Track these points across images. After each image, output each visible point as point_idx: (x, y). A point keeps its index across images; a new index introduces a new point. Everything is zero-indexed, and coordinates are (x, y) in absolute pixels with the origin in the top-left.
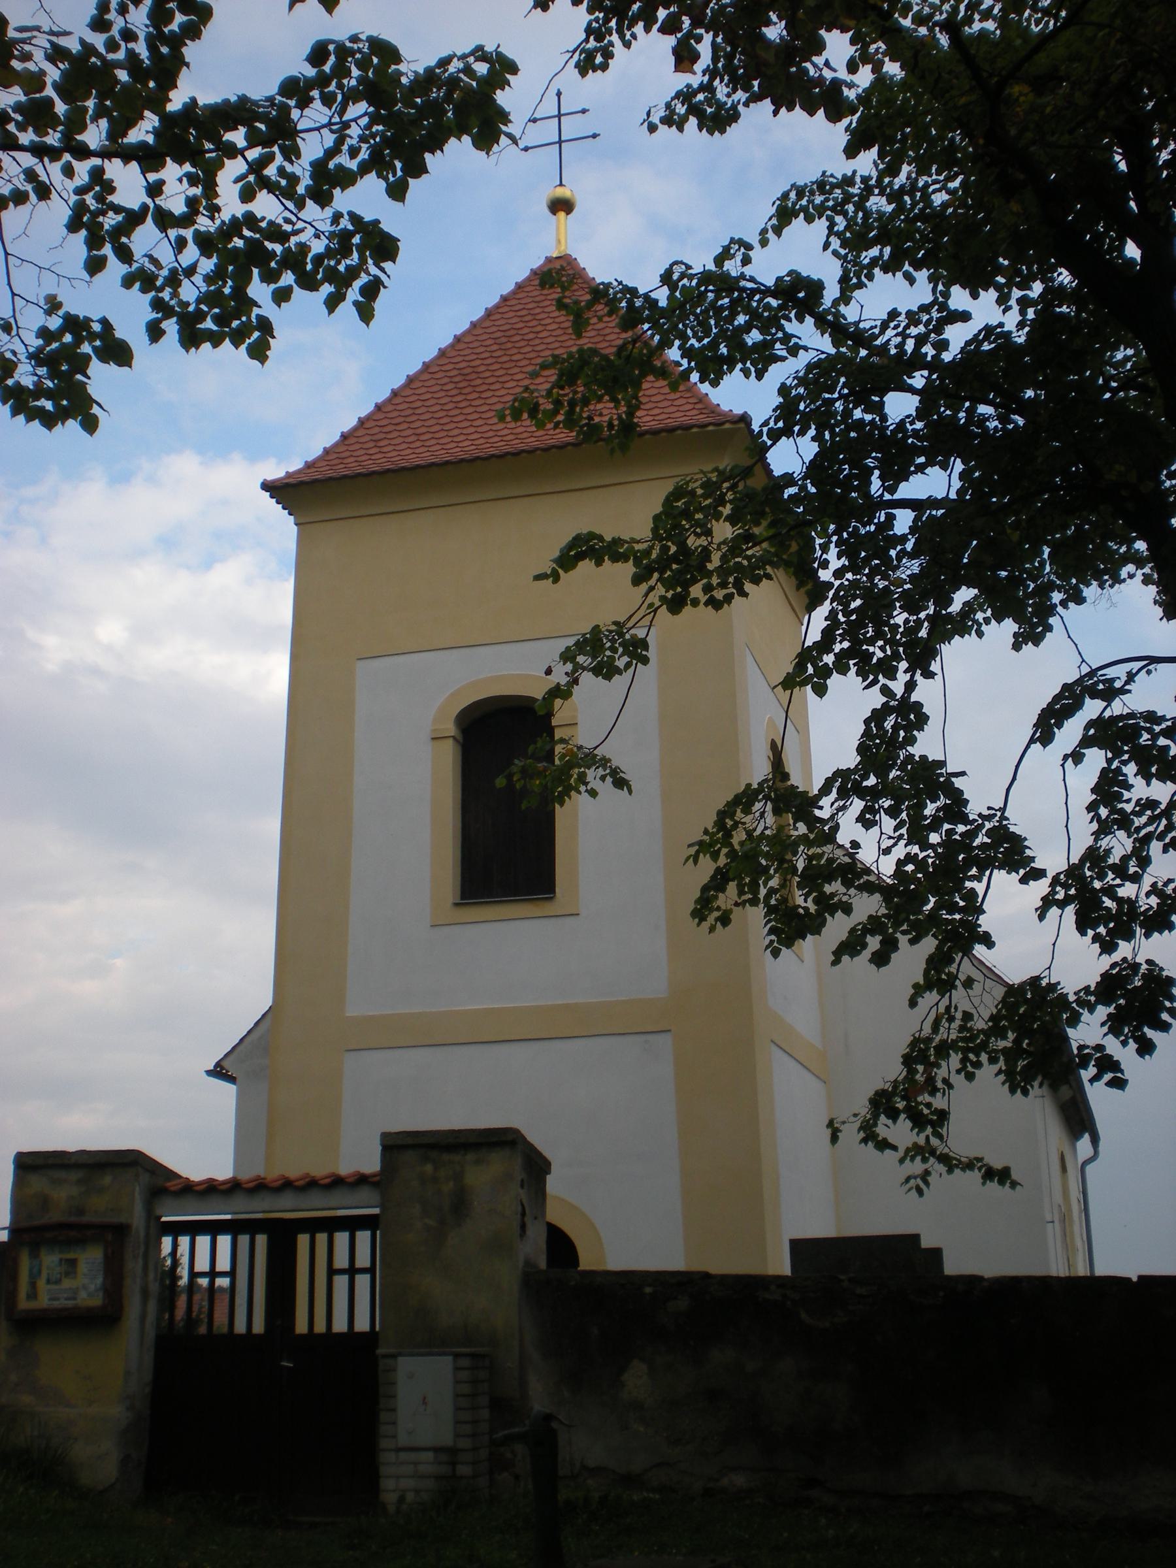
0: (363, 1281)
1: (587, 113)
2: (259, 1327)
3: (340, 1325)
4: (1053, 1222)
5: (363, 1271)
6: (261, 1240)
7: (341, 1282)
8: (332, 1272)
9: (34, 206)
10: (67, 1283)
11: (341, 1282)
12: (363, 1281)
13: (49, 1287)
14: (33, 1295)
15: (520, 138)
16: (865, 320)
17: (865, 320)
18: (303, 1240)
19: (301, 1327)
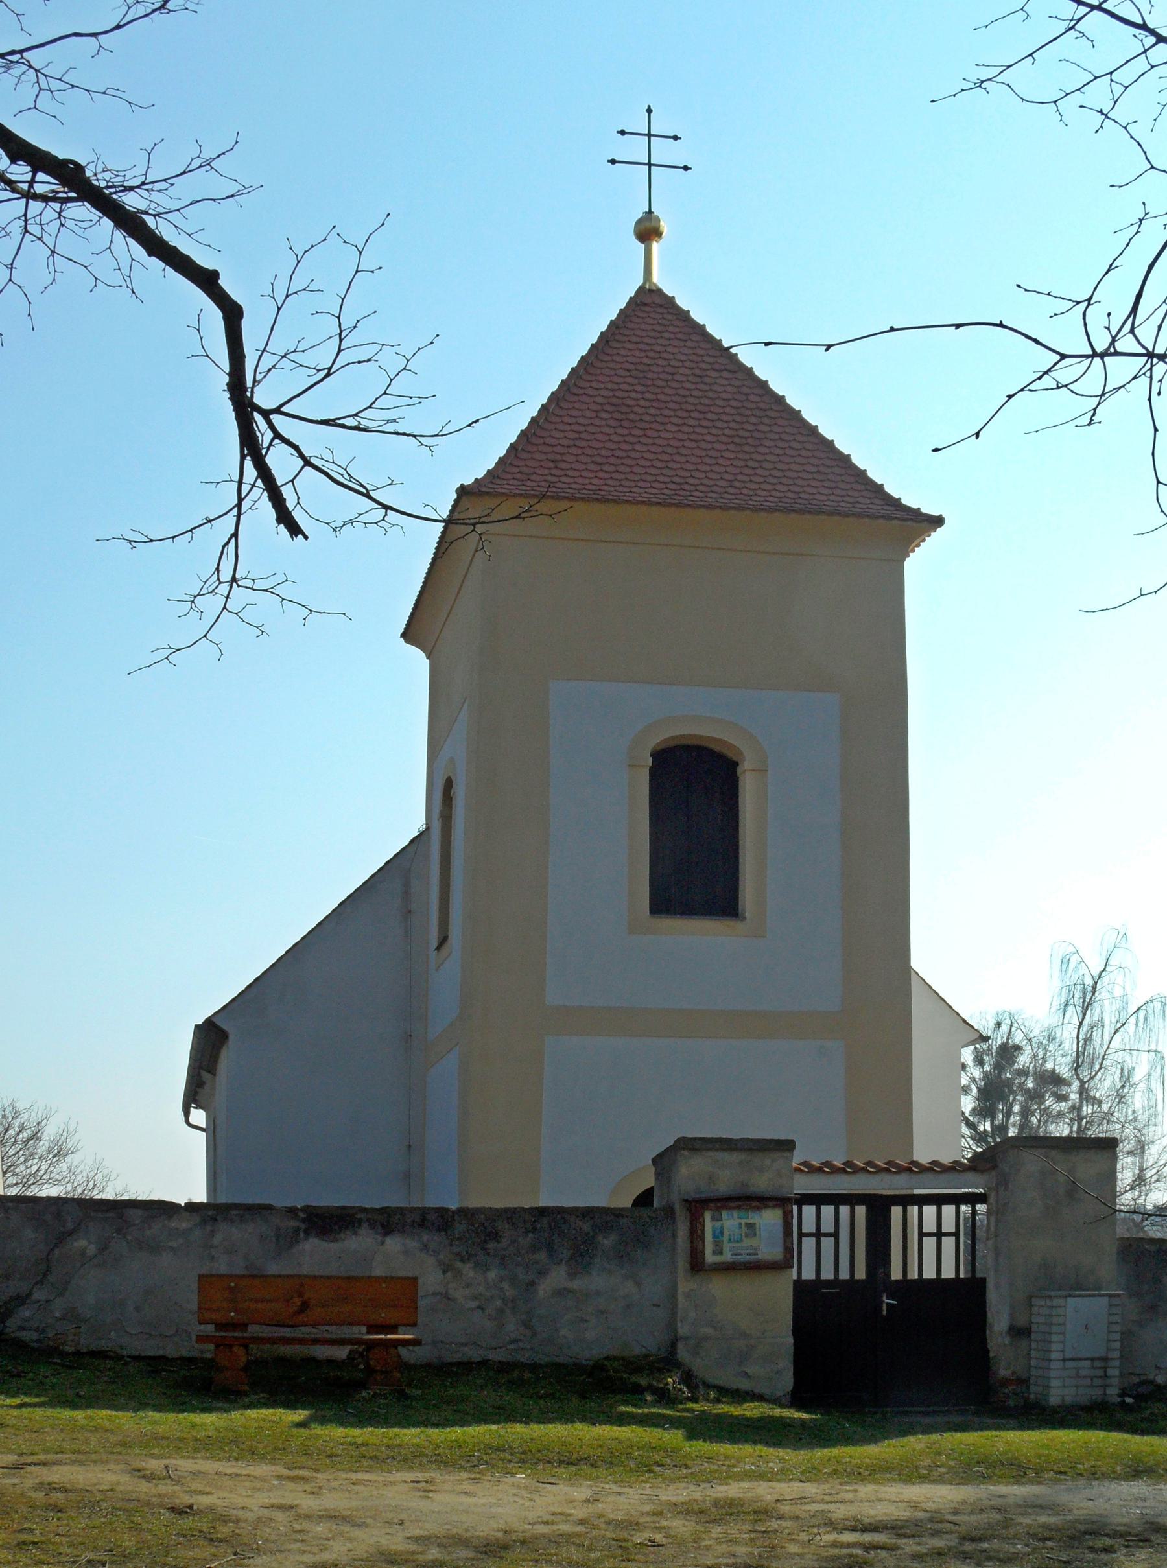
0: (948, 1243)
1: (678, 141)
2: (861, 1274)
3: (929, 1273)
4: (878, 1207)
5: (827, 1235)
6: (861, 1210)
7: (930, 1243)
8: (835, 1235)
9: (1084, 35)
10: (748, 1242)
11: (930, 1243)
12: (948, 1243)
13: (731, 1245)
14: (719, 1251)
15: (164, 270)
16: (296, 506)
17: (296, 506)
18: (896, 1211)
19: (896, 1274)
